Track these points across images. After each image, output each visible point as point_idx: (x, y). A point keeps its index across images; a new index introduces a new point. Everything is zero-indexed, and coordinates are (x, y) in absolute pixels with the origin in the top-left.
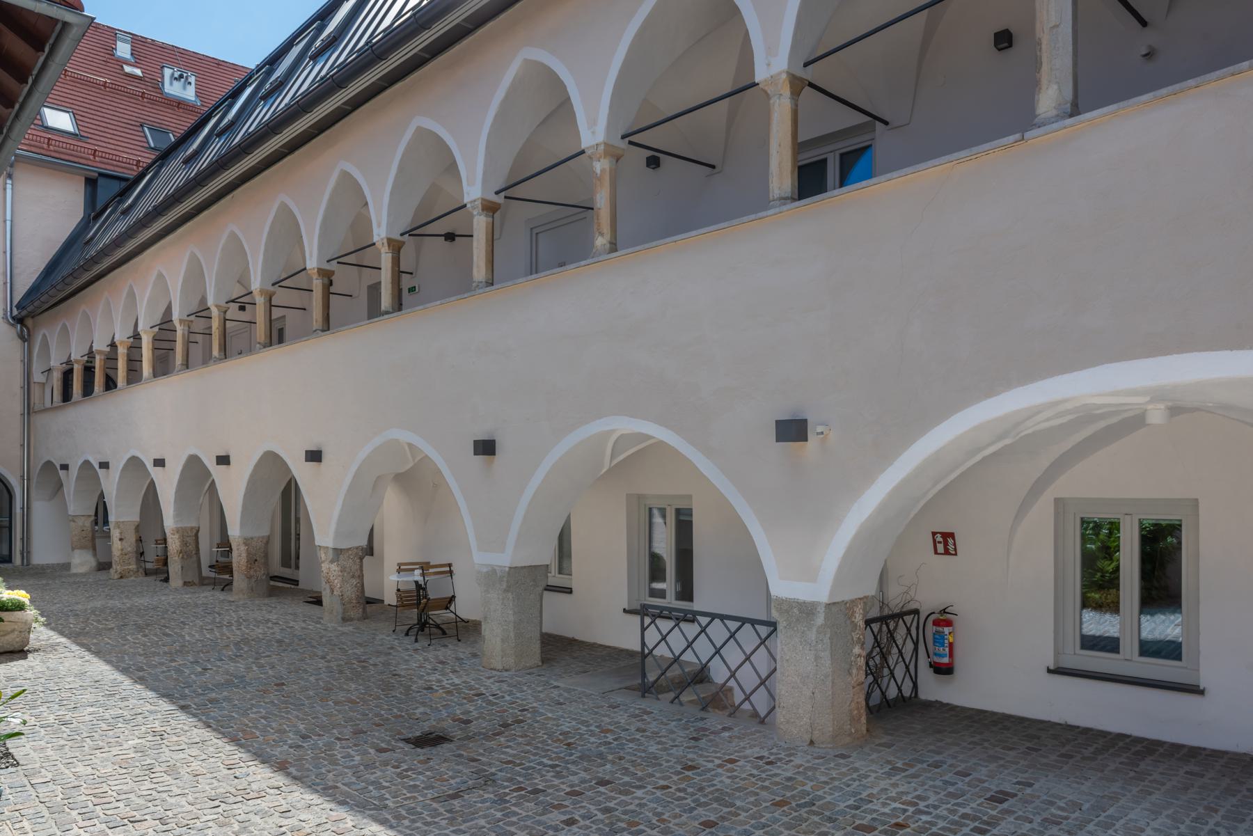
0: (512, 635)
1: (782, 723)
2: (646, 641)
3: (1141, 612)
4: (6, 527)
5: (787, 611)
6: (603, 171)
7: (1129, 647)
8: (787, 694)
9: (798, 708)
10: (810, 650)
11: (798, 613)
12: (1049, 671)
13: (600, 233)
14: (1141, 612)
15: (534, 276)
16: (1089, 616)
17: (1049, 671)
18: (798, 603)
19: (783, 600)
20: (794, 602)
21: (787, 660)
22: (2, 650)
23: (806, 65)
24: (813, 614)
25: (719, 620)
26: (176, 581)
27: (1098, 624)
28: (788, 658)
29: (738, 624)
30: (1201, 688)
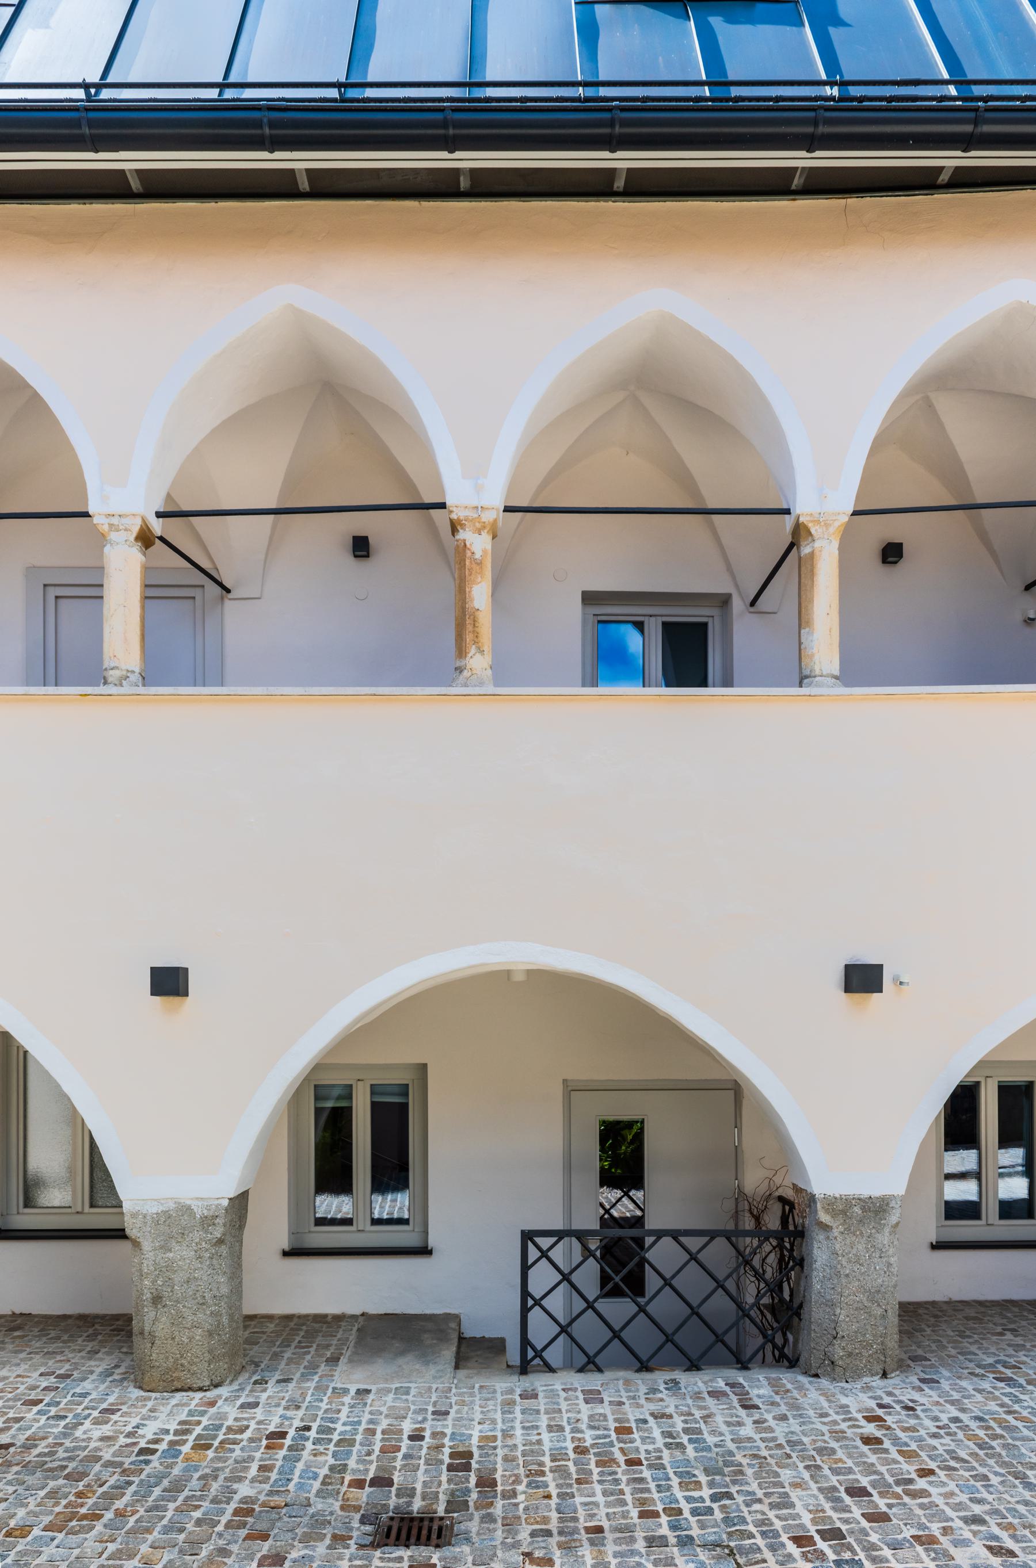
0: (225, 1320)
1: (841, 1358)
2: (531, 1289)
3: (372, 1193)
4: (596, 1300)
5: (844, 1212)
6: (485, 551)
7: (362, 1222)
8: (847, 1319)
9: (865, 1334)
10: (881, 1257)
11: (860, 1212)
12: (286, 1254)
13: (479, 648)
14: (372, 1193)
15: (51, 690)
16: (378, 1199)
17: (286, 1254)
18: (859, 1199)
19: (836, 1198)
20: (854, 1199)
21: (847, 1276)
22: (476, 3)
23: (507, 509)
24: (885, 1211)
25: (724, 1239)
26: (553, 1464)
27: (330, 1205)
28: (848, 1272)
29: (704, 1240)
30: (429, 1248)
